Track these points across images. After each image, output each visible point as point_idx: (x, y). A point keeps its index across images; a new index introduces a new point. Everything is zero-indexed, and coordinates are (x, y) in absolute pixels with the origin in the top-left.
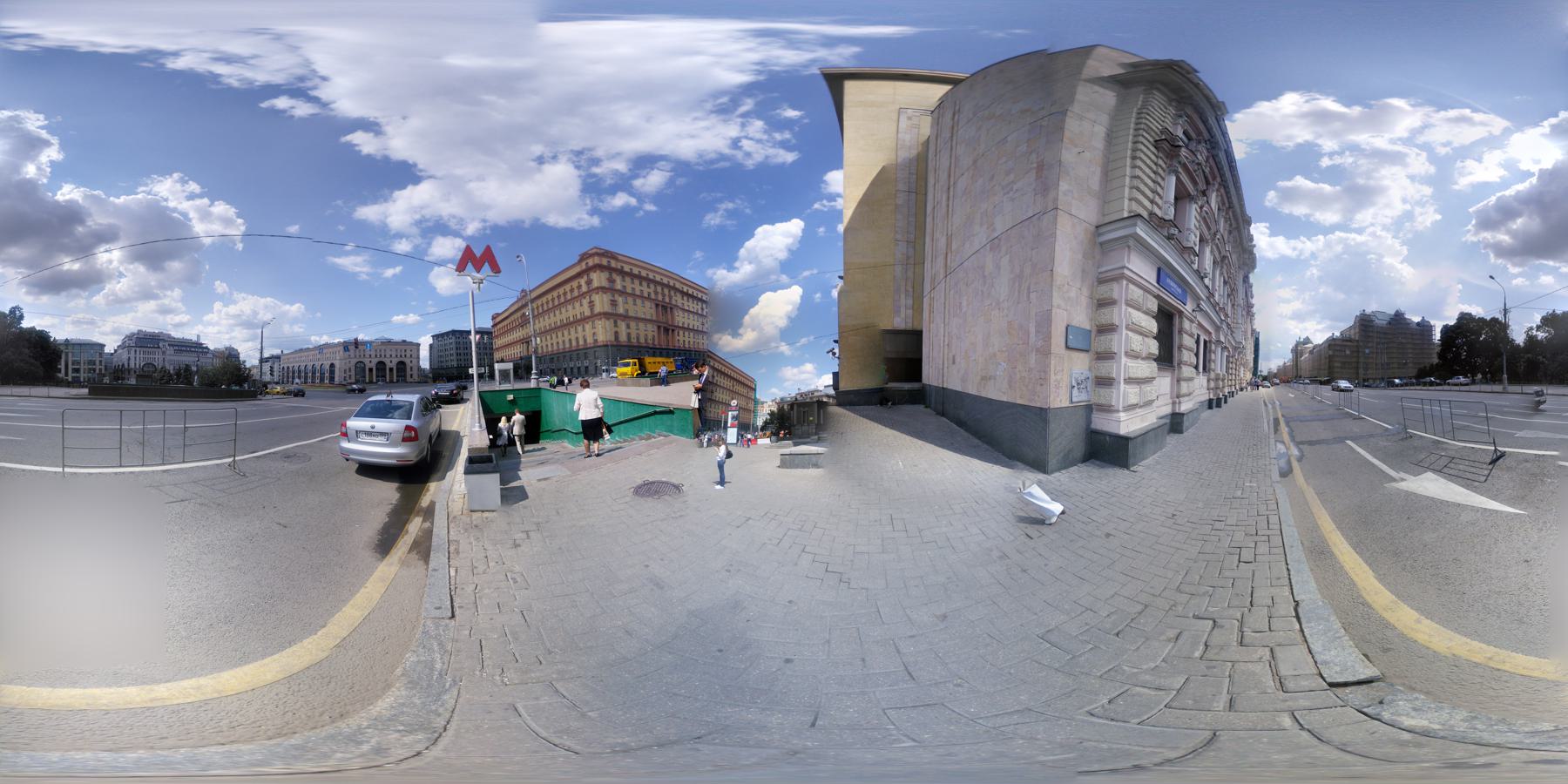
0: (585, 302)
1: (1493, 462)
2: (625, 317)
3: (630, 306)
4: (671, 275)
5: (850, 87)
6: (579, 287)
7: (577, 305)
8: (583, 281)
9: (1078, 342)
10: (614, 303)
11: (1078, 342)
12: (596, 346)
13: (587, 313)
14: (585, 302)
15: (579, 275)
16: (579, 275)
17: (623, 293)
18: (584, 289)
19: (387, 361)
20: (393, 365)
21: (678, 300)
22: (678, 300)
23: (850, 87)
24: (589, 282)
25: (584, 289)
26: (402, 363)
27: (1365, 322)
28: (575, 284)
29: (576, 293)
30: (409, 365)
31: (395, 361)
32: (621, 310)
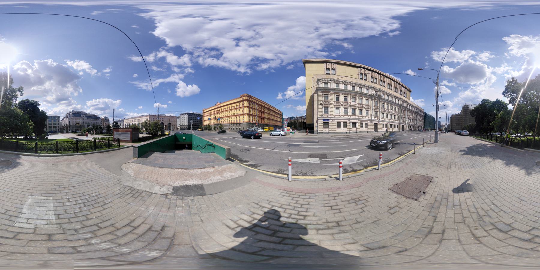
0: (241, 110)
1: (376, 146)
2: (252, 115)
3: (253, 112)
4: (272, 107)
5: (306, 65)
6: (239, 105)
7: (238, 110)
8: (241, 103)
9: (338, 84)
10: (250, 111)
11: (338, 84)
12: (243, 123)
13: (242, 113)
14: (241, 110)
15: (240, 102)
16: (240, 102)
17: (252, 108)
18: (241, 106)
19: (164, 122)
20: (167, 124)
21: (265, 110)
22: (265, 110)
23: (306, 65)
24: (243, 104)
25: (241, 106)
26: (170, 124)
27: (147, 157)
28: (238, 104)
29: (238, 107)
30: (172, 124)
31: (167, 123)
32: (251, 113)
